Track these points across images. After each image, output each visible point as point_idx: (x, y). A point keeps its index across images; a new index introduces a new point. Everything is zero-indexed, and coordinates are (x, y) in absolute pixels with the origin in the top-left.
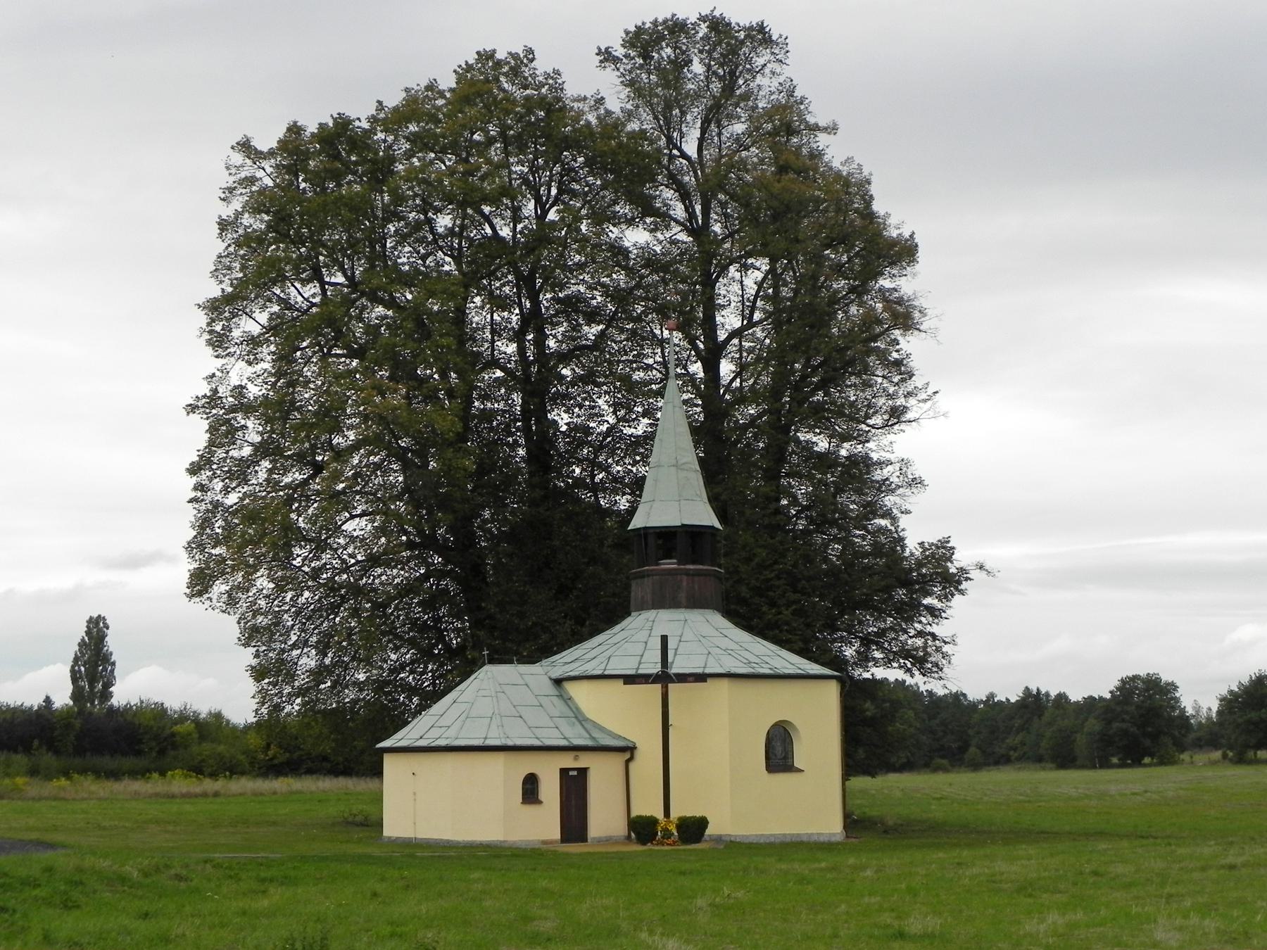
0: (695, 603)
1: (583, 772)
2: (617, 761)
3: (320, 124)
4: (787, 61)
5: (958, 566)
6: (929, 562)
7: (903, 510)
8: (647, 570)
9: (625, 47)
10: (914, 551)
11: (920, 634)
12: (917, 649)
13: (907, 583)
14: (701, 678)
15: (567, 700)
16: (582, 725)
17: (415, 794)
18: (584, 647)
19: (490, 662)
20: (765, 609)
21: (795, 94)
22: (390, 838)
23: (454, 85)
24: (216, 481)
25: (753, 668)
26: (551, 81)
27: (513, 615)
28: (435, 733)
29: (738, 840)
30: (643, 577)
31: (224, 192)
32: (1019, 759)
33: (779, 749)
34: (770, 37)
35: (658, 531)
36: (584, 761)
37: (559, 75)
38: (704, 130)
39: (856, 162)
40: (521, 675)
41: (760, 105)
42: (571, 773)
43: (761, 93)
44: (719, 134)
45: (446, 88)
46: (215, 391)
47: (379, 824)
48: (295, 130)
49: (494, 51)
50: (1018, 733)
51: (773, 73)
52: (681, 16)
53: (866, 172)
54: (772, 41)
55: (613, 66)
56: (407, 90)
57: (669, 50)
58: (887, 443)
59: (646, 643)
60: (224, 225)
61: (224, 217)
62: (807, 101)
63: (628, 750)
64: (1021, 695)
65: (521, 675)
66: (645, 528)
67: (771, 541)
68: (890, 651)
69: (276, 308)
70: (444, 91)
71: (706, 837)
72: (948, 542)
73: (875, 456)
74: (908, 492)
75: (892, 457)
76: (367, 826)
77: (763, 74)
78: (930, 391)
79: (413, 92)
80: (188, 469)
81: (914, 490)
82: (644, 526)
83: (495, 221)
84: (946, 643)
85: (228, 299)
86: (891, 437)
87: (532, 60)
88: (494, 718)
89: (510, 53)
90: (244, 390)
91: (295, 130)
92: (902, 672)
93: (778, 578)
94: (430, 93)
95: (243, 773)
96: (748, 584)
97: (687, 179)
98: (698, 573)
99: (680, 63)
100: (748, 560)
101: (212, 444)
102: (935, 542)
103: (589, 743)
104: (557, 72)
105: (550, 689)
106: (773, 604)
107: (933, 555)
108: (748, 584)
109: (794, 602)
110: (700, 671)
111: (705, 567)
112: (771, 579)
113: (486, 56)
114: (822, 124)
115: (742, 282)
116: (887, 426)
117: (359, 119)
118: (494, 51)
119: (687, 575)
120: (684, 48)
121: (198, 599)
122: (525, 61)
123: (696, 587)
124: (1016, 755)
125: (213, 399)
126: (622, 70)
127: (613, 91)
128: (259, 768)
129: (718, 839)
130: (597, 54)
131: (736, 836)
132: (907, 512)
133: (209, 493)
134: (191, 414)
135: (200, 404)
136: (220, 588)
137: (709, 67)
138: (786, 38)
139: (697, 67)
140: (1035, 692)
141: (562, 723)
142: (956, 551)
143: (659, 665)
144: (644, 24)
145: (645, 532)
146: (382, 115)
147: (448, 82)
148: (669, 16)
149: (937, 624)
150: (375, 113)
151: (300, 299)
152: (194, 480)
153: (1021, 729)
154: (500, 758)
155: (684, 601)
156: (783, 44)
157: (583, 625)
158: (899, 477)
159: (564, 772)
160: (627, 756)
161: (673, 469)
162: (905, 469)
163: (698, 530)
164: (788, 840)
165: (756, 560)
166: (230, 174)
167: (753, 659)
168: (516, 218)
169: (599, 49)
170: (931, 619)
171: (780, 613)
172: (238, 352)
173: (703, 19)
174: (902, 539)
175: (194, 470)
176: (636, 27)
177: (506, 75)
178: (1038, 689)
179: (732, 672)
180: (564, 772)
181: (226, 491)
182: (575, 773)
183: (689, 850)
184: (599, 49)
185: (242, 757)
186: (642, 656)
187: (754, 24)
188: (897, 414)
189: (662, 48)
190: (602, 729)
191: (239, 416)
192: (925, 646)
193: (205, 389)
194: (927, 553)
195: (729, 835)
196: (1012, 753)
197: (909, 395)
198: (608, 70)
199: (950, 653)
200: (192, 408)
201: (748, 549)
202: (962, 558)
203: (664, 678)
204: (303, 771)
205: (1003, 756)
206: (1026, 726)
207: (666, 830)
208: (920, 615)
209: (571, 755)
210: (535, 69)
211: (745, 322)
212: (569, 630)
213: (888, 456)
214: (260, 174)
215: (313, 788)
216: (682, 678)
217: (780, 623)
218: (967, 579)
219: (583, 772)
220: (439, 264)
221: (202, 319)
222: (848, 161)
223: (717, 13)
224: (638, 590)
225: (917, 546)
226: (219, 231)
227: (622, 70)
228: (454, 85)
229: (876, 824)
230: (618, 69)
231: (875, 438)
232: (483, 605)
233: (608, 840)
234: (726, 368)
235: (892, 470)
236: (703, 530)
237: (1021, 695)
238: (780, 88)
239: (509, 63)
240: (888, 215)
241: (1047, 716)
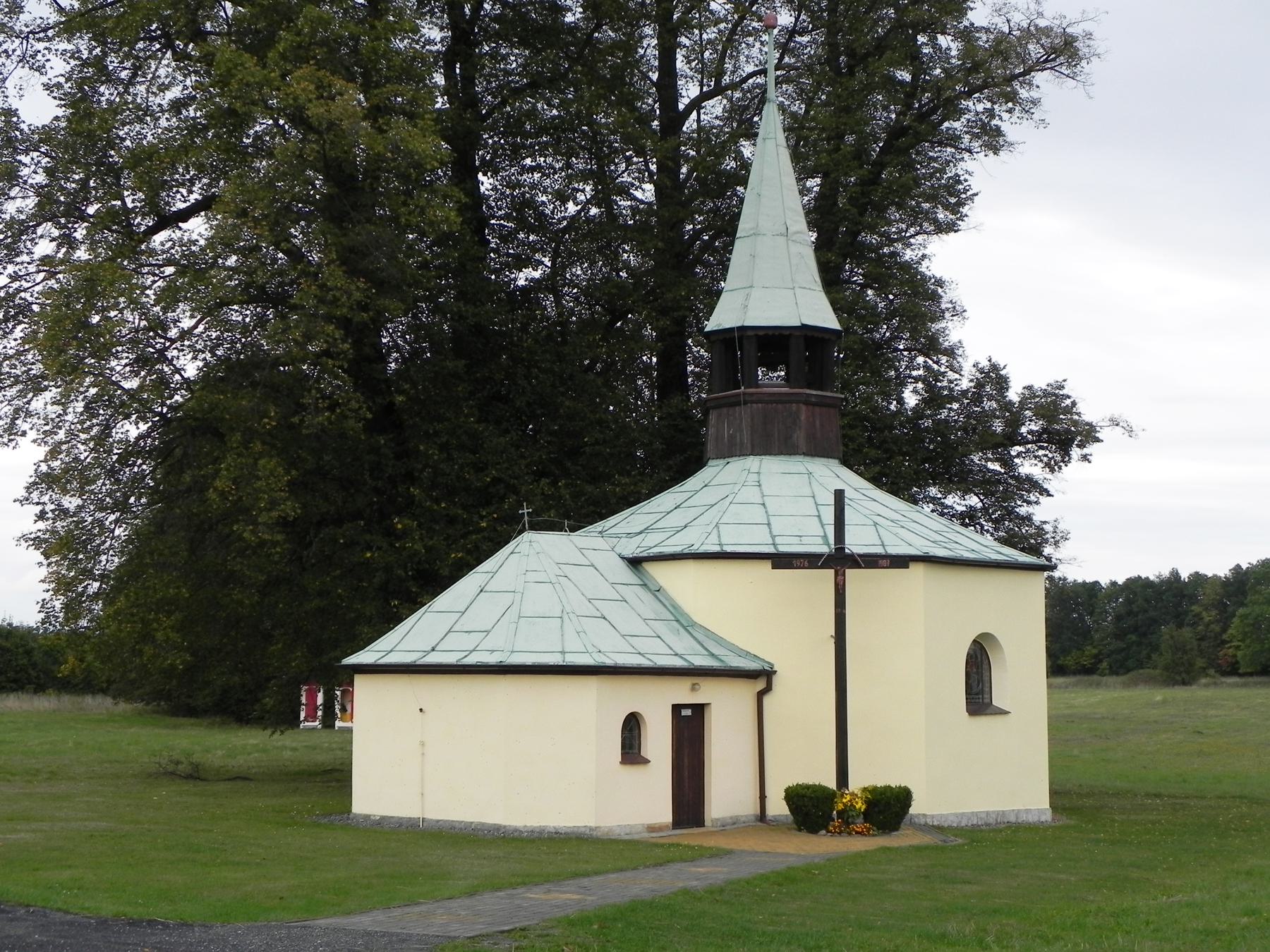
1: (699, 709)
2: (744, 692)
8: (744, 394)
15: (657, 591)
17: (422, 744)
19: (536, 527)
22: (367, 817)
28: (453, 642)
30: (738, 404)
35: (761, 333)
36: (707, 692)
63: (764, 677)
66: (742, 329)
88: (565, 617)
98: (822, 403)
105: (624, 573)
119: (807, 403)
123: (818, 423)
131: (933, 817)
141: (661, 628)
159: (677, 709)
160: (760, 685)
161: (783, 239)
163: (820, 335)
180: (677, 709)
190: (720, 641)
195: (924, 815)
209: (686, 683)
216: (871, 561)
219: (699, 709)
224: (716, 429)
236: (827, 336)
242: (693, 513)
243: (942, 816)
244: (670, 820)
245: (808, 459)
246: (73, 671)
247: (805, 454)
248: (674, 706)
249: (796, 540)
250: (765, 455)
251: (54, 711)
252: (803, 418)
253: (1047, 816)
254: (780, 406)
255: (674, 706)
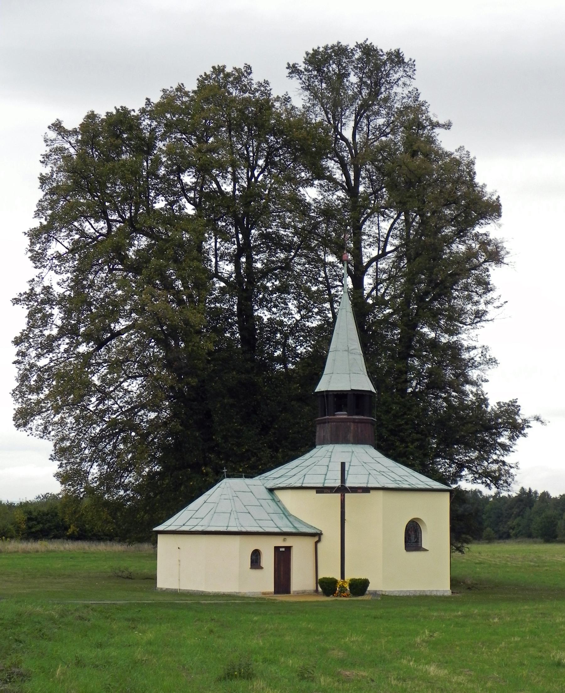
0: (358, 441)
1: (289, 549)
2: (309, 542)
3: (107, 113)
4: (414, 77)
5: (522, 418)
6: (504, 415)
7: (483, 379)
8: (328, 419)
9: (306, 64)
10: (494, 408)
11: (496, 461)
12: (495, 472)
13: (487, 428)
14: (366, 490)
15: (278, 502)
16: (288, 519)
17: (179, 561)
18: (285, 468)
19: (229, 477)
20: (398, 444)
21: (419, 99)
22: (161, 589)
23: (196, 89)
24: (31, 349)
25: (398, 484)
26: (262, 89)
27: (233, 444)
28: (193, 522)
29: (387, 594)
30: (325, 423)
31: (43, 158)
32: (516, 536)
33: (413, 536)
34: (403, 60)
35: (335, 393)
36: (289, 542)
37: (268, 84)
38: (357, 123)
39: (466, 150)
40: (247, 485)
41: (396, 106)
42: (281, 550)
43: (396, 98)
44: (368, 125)
45: (190, 90)
46: (32, 289)
47: (153, 578)
48: (92, 116)
49: (224, 67)
50: (515, 518)
51: (405, 84)
52: (344, 43)
53: (472, 157)
54: (404, 63)
55: (298, 77)
56: (164, 91)
57: (334, 66)
58: (474, 335)
59: (328, 466)
60: (43, 180)
61: (44, 174)
62: (427, 104)
63: (317, 536)
64: (519, 493)
65: (247, 485)
67: (403, 400)
68: (477, 473)
69: (77, 237)
70: (189, 92)
71: (367, 592)
72: (516, 402)
73: (465, 344)
74: (486, 367)
75: (478, 345)
76: (131, 579)
77: (398, 85)
78: (502, 301)
79: (168, 92)
80: (13, 342)
81: (490, 366)
82: (326, 390)
83: (218, 180)
84: (511, 467)
85: (44, 229)
86: (476, 331)
87: (249, 74)
88: (232, 513)
89: (235, 68)
90: (51, 290)
91: (92, 116)
92: (483, 486)
93: (406, 423)
94: (179, 93)
95: (12, 537)
96: (386, 428)
97: (345, 154)
98: (361, 422)
99: (342, 76)
100: (388, 412)
101: (31, 327)
102: (507, 402)
103: (293, 530)
104: (267, 82)
105: (267, 495)
106: (402, 441)
107: (506, 411)
108: (386, 428)
109: (417, 440)
110: (364, 485)
111: (365, 418)
112: (402, 425)
113: (218, 70)
114: (441, 122)
115: (378, 224)
116: (473, 323)
117: (134, 110)
118: (224, 67)
120: (344, 65)
121: (23, 429)
122: (245, 74)
123: (359, 430)
124: (514, 532)
125: (30, 296)
126: (303, 79)
127: (296, 93)
128: (23, 534)
129: (375, 593)
130: (287, 68)
131: (386, 591)
132: (487, 381)
133: (26, 358)
134: (15, 305)
135: (22, 298)
136: (38, 421)
137: (361, 79)
138: (414, 61)
139: (353, 79)
140: (527, 491)
142: (521, 408)
143: (340, 481)
144: (319, 48)
145: (326, 394)
146: (149, 109)
147: (191, 86)
148: (335, 43)
149: (506, 455)
150: (144, 107)
151: (92, 231)
152: (16, 349)
153: (518, 515)
154: (237, 539)
155: (351, 439)
156: (412, 65)
157: (277, 451)
158: (480, 357)
159: (277, 549)
160: (316, 539)
161: (347, 352)
162: (485, 353)
163: (361, 393)
164: (418, 594)
165: (393, 412)
166: (47, 145)
167: (398, 478)
168: (235, 180)
169: (289, 64)
170: (502, 452)
171: (407, 447)
172: (50, 265)
173: (359, 46)
174: (486, 400)
175: (17, 342)
176: (313, 50)
177: (232, 83)
178: (530, 489)
179: (386, 486)
180: (277, 549)
181: (39, 356)
182: (283, 549)
183: (358, 600)
184: (289, 64)
185: (11, 527)
186: (326, 475)
187: (393, 50)
188: (479, 315)
189: (330, 65)
190: (300, 521)
191: (47, 307)
192: (499, 470)
193: (26, 288)
194: (502, 409)
196: (511, 531)
197: (487, 303)
198: (294, 79)
199: (514, 474)
200: (16, 301)
201: (387, 404)
202: (525, 413)
203: (342, 490)
204: (51, 537)
205: (505, 533)
206: (521, 513)
207: (342, 587)
208: (496, 449)
209: (281, 538)
210: (252, 79)
211: (380, 252)
212: (269, 455)
213: (473, 344)
214: (67, 146)
215: (62, 548)
216: (354, 490)
217: (407, 453)
218: (528, 427)
220: (181, 208)
221: (27, 241)
222: (461, 148)
223: (368, 43)
224: (320, 432)
225: (496, 405)
226: (40, 184)
227: (303, 79)
228: (196, 89)
229: (460, 583)
230: (301, 79)
231: (466, 332)
232: (214, 437)
233: (303, 593)
234: (368, 281)
235: (476, 353)
236: (364, 394)
237: (519, 493)
238: (409, 95)
239: (234, 74)
240: (484, 186)
241: (535, 507)
242: (302, 468)
243: (390, 591)
244: (273, 590)
245: (354, 445)
246: (73, 533)
247: (352, 443)
248: (275, 547)
249: (333, 481)
250: (336, 444)
251: (124, 552)
252: (352, 428)
253: (449, 593)
254: (343, 424)
255: (275, 547)
